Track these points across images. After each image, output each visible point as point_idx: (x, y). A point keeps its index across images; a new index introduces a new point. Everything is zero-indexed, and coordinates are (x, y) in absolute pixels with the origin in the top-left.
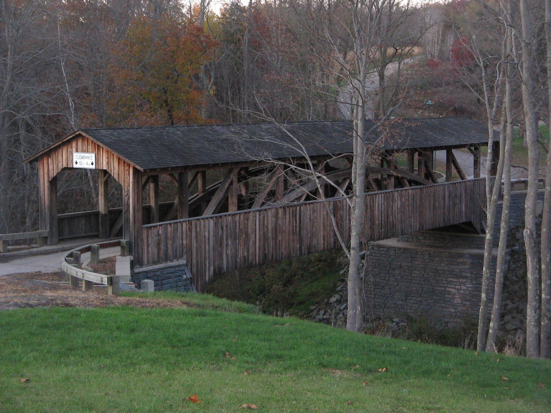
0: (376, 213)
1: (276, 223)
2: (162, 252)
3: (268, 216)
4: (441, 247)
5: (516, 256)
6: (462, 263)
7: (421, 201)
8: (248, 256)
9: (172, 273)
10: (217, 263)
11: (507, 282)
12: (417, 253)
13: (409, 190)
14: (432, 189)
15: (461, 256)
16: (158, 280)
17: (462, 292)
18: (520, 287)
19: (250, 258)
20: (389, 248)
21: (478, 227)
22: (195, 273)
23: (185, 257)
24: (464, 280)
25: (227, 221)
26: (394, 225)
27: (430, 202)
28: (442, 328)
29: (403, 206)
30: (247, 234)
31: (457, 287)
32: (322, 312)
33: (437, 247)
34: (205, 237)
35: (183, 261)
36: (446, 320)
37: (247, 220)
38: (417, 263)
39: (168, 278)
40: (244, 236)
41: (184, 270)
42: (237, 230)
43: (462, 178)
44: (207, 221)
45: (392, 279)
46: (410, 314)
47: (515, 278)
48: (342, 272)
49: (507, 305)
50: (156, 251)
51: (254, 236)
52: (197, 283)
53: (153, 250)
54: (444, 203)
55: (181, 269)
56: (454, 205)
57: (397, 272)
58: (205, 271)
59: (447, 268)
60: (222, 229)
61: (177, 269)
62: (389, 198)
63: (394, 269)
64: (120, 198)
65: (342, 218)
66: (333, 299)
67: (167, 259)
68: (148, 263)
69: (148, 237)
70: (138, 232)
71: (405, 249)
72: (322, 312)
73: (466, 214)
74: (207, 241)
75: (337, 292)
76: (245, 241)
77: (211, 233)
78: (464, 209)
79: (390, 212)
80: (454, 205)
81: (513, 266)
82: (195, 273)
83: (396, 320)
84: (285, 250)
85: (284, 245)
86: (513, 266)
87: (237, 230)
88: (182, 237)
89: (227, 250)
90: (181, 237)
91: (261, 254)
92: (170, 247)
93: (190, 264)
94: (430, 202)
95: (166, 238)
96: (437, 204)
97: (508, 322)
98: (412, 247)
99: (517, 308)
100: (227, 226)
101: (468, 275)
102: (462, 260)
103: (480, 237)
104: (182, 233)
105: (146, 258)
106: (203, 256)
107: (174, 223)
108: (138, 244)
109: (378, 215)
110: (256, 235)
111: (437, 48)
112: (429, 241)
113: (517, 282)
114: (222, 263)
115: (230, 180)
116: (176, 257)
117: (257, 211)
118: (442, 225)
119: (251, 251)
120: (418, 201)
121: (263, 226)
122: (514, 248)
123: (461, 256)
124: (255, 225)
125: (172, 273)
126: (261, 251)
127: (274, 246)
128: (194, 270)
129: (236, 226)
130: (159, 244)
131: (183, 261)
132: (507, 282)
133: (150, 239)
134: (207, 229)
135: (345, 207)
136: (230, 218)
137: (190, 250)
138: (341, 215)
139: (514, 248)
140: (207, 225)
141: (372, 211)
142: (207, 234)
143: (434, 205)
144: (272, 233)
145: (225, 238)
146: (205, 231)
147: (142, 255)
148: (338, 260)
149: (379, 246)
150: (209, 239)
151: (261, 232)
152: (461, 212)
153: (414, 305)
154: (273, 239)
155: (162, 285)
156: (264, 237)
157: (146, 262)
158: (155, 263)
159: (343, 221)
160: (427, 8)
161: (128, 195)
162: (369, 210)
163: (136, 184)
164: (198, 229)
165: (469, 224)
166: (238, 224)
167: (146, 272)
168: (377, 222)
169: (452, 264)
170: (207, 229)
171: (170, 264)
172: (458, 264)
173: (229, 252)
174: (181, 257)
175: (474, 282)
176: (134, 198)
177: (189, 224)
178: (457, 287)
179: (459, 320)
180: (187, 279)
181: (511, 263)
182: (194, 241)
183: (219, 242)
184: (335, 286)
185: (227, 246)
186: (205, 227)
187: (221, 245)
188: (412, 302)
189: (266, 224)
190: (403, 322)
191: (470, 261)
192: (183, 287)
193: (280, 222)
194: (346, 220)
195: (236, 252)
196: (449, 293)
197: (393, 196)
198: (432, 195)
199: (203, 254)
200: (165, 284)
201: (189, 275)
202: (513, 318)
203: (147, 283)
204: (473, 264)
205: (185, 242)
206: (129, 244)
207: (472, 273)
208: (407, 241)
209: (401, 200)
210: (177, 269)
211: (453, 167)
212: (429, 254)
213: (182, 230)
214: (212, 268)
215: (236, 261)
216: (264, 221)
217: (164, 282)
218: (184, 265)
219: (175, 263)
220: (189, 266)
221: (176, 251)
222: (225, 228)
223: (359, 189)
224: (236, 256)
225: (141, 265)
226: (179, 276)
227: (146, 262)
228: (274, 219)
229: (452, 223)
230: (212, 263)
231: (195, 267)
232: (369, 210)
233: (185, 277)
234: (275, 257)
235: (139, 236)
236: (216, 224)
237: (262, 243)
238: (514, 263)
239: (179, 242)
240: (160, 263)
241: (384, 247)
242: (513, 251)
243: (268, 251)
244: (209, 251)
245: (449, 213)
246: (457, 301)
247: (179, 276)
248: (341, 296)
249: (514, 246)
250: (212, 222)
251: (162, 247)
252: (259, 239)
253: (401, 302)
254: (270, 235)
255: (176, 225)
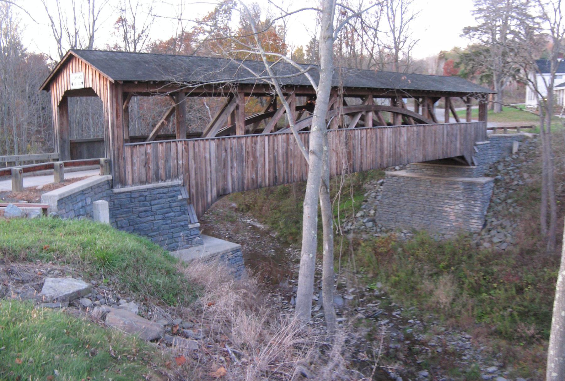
0: (385, 145)
1: (287, 149)
2: (151, 173)
3: (278, 141)
4: (440, 176)
5: (499, 184)
6: (456, 188)
7: (424, 137)
8: (257, 178)
9: (164, 193)
10: (221, 185)
11: (492, 204)
12: (421, 180)
13: (415, 128)
14: (434, 128)
15: (455, 183)
16: (145, 201)
17: (456, 211)
18: (503, 208)
19: (259, 180)
20: (400, 177)
21: (469, 161)
22: (195, 194)
23: (181, 177)
24: (458, 202)
25: (232, 144)
26: (401, 155)
27: (431, 137)
28: (440, 239)
29: (408, 139)
30: (255, 157)
31: (452, 207)
32: (350, 224)
33: (437, 176)
34: (205, 158)
35: (178, 182)
36: (443, 232)
37: (255, 144)
38: (421, 188)
39: (159, 199)
40: (252, 159)
41: (179, 190)
42: (244, 153)
43: (457, 121)
44: (207, 143)
45: (402, 200)
46: (415, 227)
47: (499, 201)
48: (366, 195)
49: (492, 222)
50: (143, 171)
51: (262, 159)
52: (197, 205)
53: (139, 169)
54: (443, 139)
55: (176, 189)
56: (451, 142)
57: (406, 195)
58: (207, 192)
59: (444, 193)
60: (226, 151)
61: (170, 189)
62: (398, 134)
63: (403, 193)
64: (101, 115)
65: (354, 147)
66: (359, 215)
67: (158, 178)
68: (134, 183)
69: (132, 156)
70: (118, 149)
71: (412, 178)
72: (350, 224)
73: (460, 149)
74: (208, 163)
75: (362, 210)
76: (252, 163)
77: (213, 155)
78: (458, 146)
79: (397, 144)
80: (451, 142)
81: (497, 191)
82: (195, 194)
83: (405, 231)
84: (297, 173)
85: (295, 169)
86: (497, 191)
87: (244, 153)
88: (177, 157)
89: (232, 171)
90: (175, 157)
91: (272, 178)
92: (161, 166)
93: (188, 184)
94: (431, 137)
95: (156, 157)
96: (437, 140)
97: (494, 236)
98: (417, 176)
99: (501, 225)
100: (231, 149)
101: (461, 198)
102: (456, 186)
103: (470, 169)
104: (177, 152)
105: (130, 177)
106: (204, 177)
107: (166, 142)
108: (118, 161)
109: (387, 146)
110: (264, 158)
111: (435, 69)
112: (430, 172)
113: (500, 203)
114: (227, 185)
115: (235, 105)
116: (168, 177)
117: (266, 135)
118: (441, 158)
119: (260, 173)
120: (422, 137)
121: (273, 150)
122: (497, 177)
123: (455, 183)
124: (264, 149)
125: (164, 193)
126: (271, 174)
127: (285, 169)
128: (193, 191)
129: (242, 149)
130: (147, 164)
131: (178, 182)
132: (492, 204)
133: (135, 157)
134: (208, 150)
135: (357, 137)
136: (235, 140)
137: (188, 170)
138: (353, 144)
139: (497, 177)
140: (207, 146)
141: (382, 143)
142: (208, 156)
143: (435, 140)
144: (283, 158)
145: (229, 159)
146: (205, 152)
147: (125, 174)
148: (364, 186)
149: (392, 176)
150: (210, 161)
151: (271, 156)
152: (456, 148)
153: (418, 220)
154: (284, 163)
155: (151, 205)
156: (275, 160)
157: (130, 181)
158: (142, 183)
159: (355, 149)
160: (428, 59)
161: (107, 111)
162: (379, 141)
163: (114, 99)
164: (197, 150)
165: (462, 157)
166: (244, 147)
167: (130, 192)
168: (386, 152)
169: (447, 190)
170: (208, 150)
171: (161, 184)
172: (454, 189)
173: (235, 173)
174: (177, 177)
175: (466, 203)
176: (112, 114)
177: (185, 144)
178: (452, 207)
179: (453, 233)
180: (184, 199)
181: (495, 189)
182: (192, 162)
183: (223, 164)
184: (361, 205)
185: (231, 168)
186: (205, 148)
187: (225, 166)
188: (417, 218)
189: (276, 148)
190: (410, 233)
191: (462, 187)
192: (179, 208)
193: (291, 147)
194: (358, 149)
195: (242, 173)
196: (446, 211)
197: (400, 131)
198: (433, 132)
199: (204, 175)
200: (154, 205)
201: (185, 195)
202: (498, 232)
203: (98, 205)
204: (465, 189)
205: (180, 162)
206: (108, 162)
207: (464, 196)
208: (413, 172)
209: (407, 134)
210: (170, 189)
211: (450, 111)
212: (431, 181)
213: (177, 149)
214: (215, 189)
215: (243, 183)
216: (274, 145)
217: (153, 202)
218: (179, 185)
219: (169, 183)
220: (187, 186)
221: (170, 171)
222: (229, 150)
223: (325, 60)
224: (243, 179)
225: (123, 183)
226: (174, 196)
227: (130, 181)
228: (285, 144)
229: (449, 156)
230: (215, 184)
231: (194, 188)
232: (379, 141)
233: (180, 197)
234: (286, 178)
235: (120, 154)
236: (218, 146)
237: (272, 167)
238: (497, 189)
239: (172, 162)
240: (149, 183)
241: (395, 176)
242: (496, 179)
243: (279, 174)
244: (211, 172)
245: (447, 148)
246: (452, 218)
247: (174, 196)
248: (364, 212)
249: (497, 175)
250: (213, 144)
251: (151, 166)
252: (269, 162)
253: (408, 218)
254: (281, 159)
255: (169, 145)
